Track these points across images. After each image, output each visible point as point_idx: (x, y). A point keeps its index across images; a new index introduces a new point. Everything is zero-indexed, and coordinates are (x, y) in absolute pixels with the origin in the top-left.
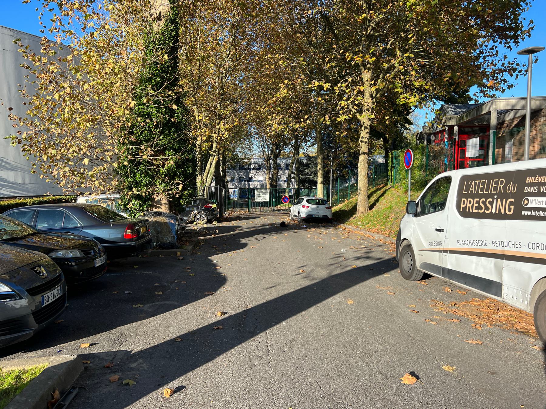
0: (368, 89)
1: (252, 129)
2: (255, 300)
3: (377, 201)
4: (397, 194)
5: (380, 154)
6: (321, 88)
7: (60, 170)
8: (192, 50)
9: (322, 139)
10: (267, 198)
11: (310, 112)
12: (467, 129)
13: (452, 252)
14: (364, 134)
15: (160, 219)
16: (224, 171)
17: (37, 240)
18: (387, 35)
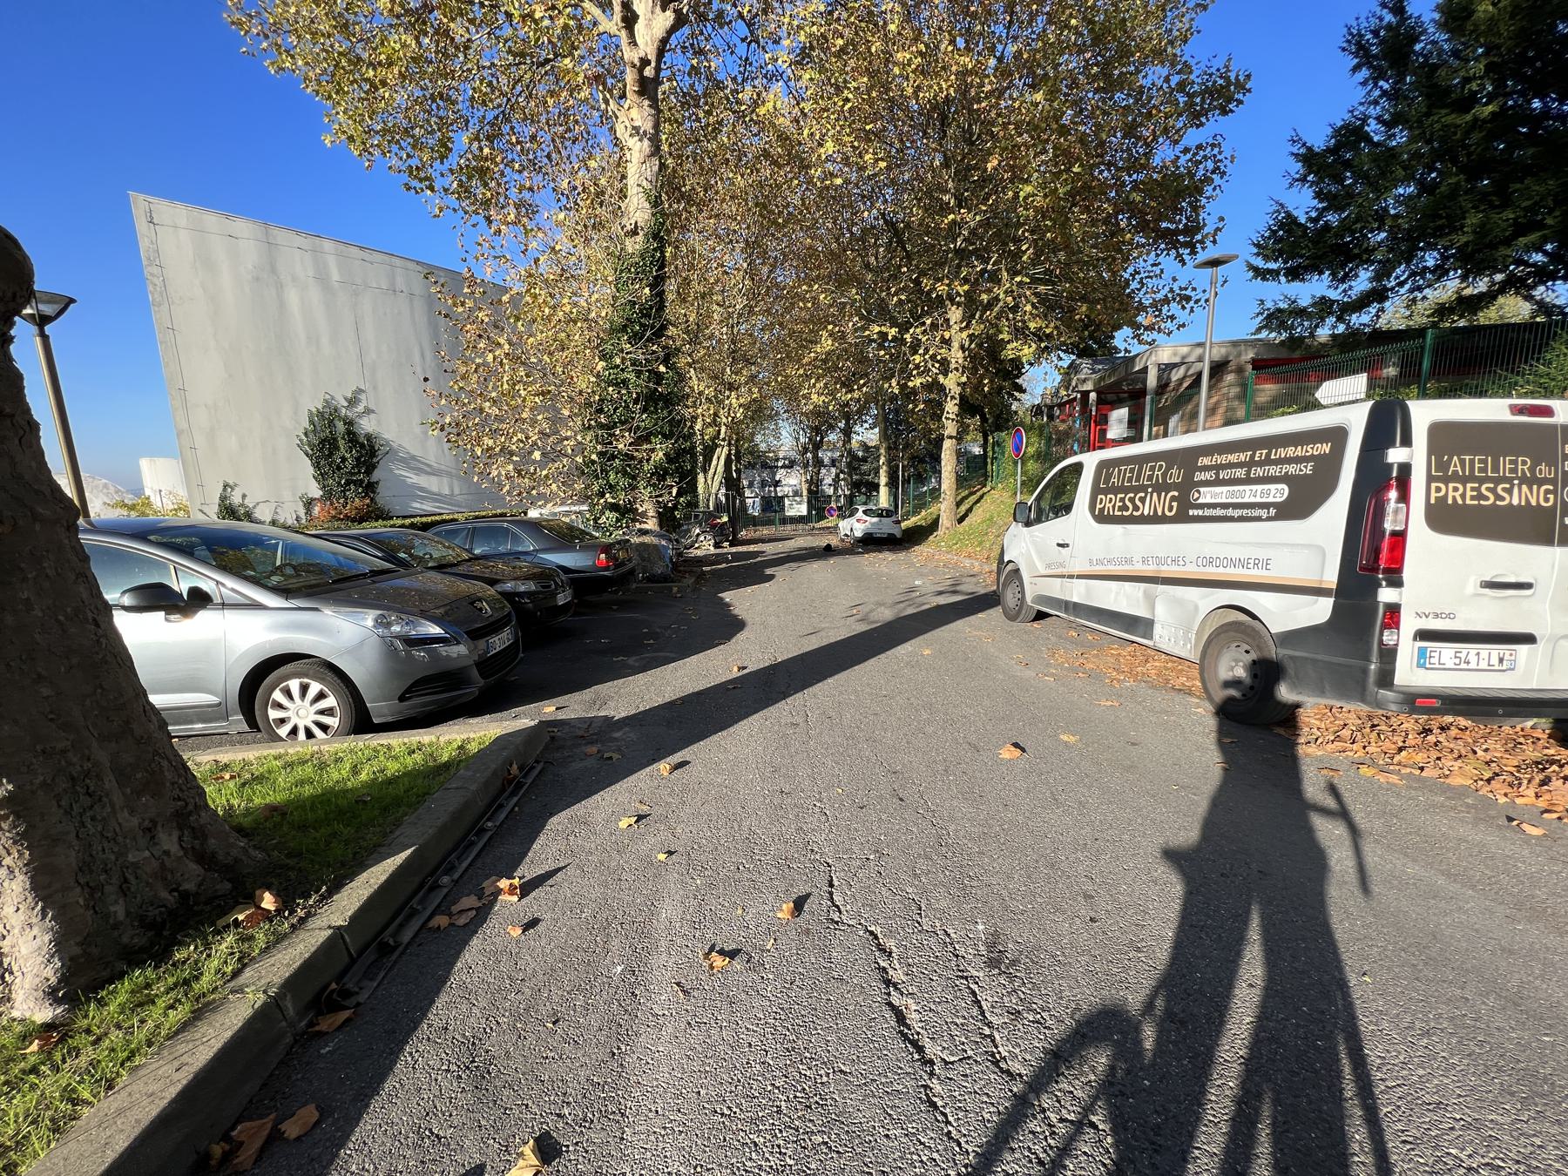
0: (958, 337)
1: (778, 405)
2: (787, 648)
3: (970, 510)
4: (998, 498)
5: (975, 440)
6: (883, 335)
7: (501, 469)
8: (687, 282)
9: (886, 419)
10: (802, 509)
11: (867, 375)
12: (1111, 397)
13: (1079, 577)
14: (951, 408)
15: (647, 539)
16: (738, 471)
17: (476, 568)
18: (987, 249)
